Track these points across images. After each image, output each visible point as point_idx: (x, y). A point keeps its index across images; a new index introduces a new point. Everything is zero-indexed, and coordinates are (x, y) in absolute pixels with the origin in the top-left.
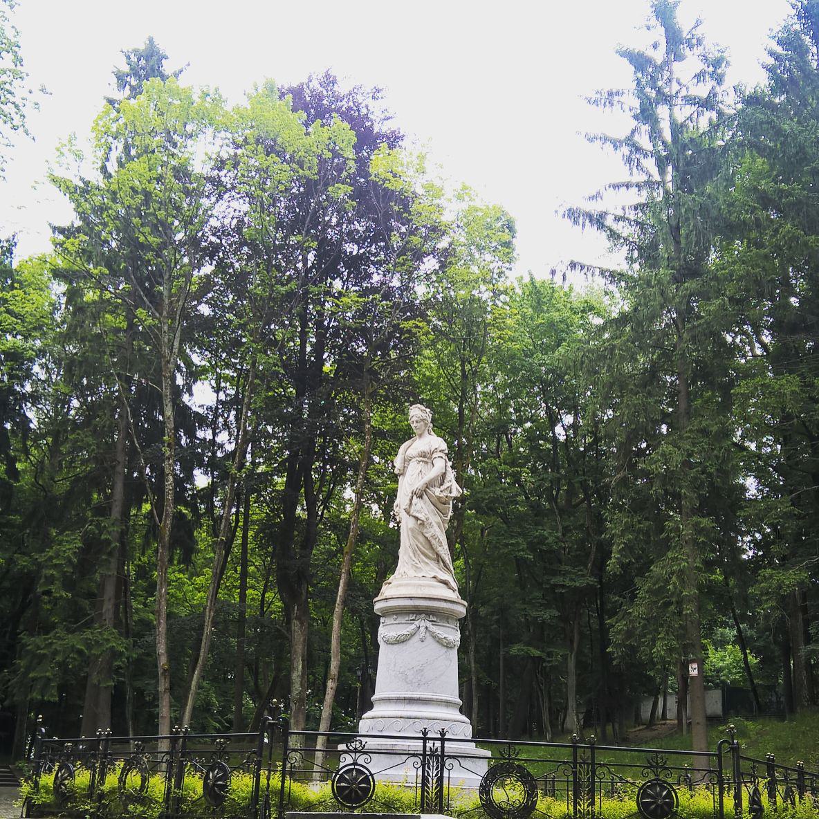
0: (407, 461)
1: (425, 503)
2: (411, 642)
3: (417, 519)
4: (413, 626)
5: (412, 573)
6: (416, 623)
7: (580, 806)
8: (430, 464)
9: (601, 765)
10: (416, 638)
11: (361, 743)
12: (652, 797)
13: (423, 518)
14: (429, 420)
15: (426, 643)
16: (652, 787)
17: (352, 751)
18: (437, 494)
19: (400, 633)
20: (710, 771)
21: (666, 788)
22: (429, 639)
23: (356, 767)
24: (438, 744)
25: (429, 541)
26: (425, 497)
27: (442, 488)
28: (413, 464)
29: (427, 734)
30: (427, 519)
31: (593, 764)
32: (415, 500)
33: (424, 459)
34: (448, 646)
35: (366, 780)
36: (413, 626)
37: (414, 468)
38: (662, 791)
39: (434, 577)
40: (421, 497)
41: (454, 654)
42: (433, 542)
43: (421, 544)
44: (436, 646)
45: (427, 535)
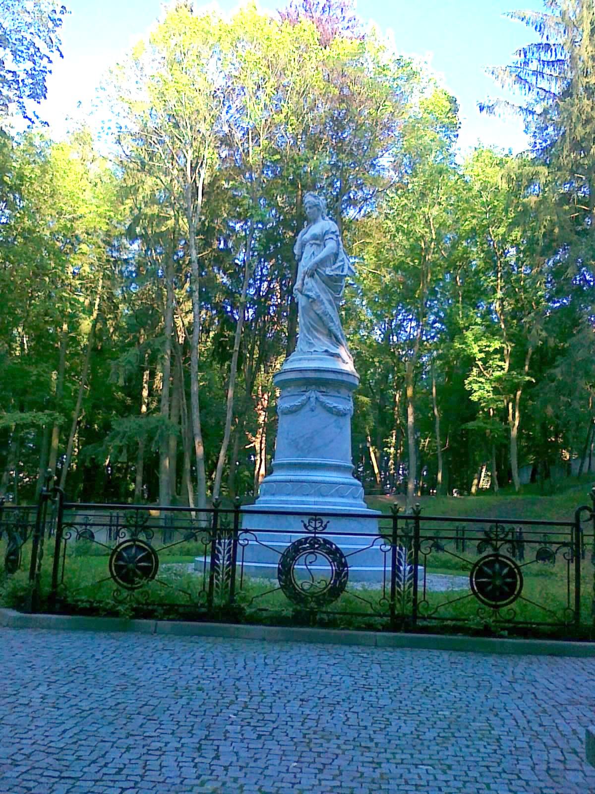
0: (303, 246)
1: (316, 282)
2: (303, 411)
3: (308, 297)
4: (304, 397)
5: (306, 349)
6: (307, 394)
7: (399, 586)
8: (322, 247)
9: (246, 531)
10: (307, 408)
11: (322, 522)
12: (488, 576)
13: (314, 296)
14: (74, 215)
15: (316, 412)
16: (490, 564)
17: (132, 526)
18: (327, 273)
19: (292, 404)
20: (383, 536)
21: (507, 565)
22: (319, 409)
23: (137, 543)
24: (231, 517)
25: (321, 318)
26: (316, 276)
27: (334, 267)
28: (308, 248)
29: (218, 505)
30: (319, 296)
31: (417, 536)
32: (307, 279)
33: (318, 242)
34: (341, 414)
35: (511, 574)
36: (304, 397)
37: (308, 250)
38: (502, 569)
39: (326, 351)
40: (312, 276)
41: (347, 423)
42: (325, 318)
43: (313, 320)
44: (325, 414)
45: (318, 312)
